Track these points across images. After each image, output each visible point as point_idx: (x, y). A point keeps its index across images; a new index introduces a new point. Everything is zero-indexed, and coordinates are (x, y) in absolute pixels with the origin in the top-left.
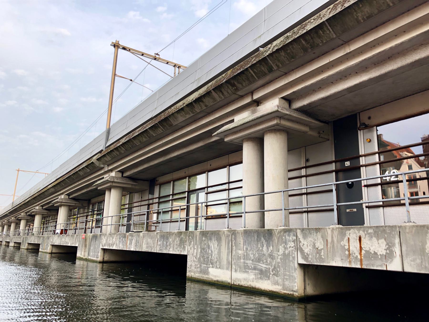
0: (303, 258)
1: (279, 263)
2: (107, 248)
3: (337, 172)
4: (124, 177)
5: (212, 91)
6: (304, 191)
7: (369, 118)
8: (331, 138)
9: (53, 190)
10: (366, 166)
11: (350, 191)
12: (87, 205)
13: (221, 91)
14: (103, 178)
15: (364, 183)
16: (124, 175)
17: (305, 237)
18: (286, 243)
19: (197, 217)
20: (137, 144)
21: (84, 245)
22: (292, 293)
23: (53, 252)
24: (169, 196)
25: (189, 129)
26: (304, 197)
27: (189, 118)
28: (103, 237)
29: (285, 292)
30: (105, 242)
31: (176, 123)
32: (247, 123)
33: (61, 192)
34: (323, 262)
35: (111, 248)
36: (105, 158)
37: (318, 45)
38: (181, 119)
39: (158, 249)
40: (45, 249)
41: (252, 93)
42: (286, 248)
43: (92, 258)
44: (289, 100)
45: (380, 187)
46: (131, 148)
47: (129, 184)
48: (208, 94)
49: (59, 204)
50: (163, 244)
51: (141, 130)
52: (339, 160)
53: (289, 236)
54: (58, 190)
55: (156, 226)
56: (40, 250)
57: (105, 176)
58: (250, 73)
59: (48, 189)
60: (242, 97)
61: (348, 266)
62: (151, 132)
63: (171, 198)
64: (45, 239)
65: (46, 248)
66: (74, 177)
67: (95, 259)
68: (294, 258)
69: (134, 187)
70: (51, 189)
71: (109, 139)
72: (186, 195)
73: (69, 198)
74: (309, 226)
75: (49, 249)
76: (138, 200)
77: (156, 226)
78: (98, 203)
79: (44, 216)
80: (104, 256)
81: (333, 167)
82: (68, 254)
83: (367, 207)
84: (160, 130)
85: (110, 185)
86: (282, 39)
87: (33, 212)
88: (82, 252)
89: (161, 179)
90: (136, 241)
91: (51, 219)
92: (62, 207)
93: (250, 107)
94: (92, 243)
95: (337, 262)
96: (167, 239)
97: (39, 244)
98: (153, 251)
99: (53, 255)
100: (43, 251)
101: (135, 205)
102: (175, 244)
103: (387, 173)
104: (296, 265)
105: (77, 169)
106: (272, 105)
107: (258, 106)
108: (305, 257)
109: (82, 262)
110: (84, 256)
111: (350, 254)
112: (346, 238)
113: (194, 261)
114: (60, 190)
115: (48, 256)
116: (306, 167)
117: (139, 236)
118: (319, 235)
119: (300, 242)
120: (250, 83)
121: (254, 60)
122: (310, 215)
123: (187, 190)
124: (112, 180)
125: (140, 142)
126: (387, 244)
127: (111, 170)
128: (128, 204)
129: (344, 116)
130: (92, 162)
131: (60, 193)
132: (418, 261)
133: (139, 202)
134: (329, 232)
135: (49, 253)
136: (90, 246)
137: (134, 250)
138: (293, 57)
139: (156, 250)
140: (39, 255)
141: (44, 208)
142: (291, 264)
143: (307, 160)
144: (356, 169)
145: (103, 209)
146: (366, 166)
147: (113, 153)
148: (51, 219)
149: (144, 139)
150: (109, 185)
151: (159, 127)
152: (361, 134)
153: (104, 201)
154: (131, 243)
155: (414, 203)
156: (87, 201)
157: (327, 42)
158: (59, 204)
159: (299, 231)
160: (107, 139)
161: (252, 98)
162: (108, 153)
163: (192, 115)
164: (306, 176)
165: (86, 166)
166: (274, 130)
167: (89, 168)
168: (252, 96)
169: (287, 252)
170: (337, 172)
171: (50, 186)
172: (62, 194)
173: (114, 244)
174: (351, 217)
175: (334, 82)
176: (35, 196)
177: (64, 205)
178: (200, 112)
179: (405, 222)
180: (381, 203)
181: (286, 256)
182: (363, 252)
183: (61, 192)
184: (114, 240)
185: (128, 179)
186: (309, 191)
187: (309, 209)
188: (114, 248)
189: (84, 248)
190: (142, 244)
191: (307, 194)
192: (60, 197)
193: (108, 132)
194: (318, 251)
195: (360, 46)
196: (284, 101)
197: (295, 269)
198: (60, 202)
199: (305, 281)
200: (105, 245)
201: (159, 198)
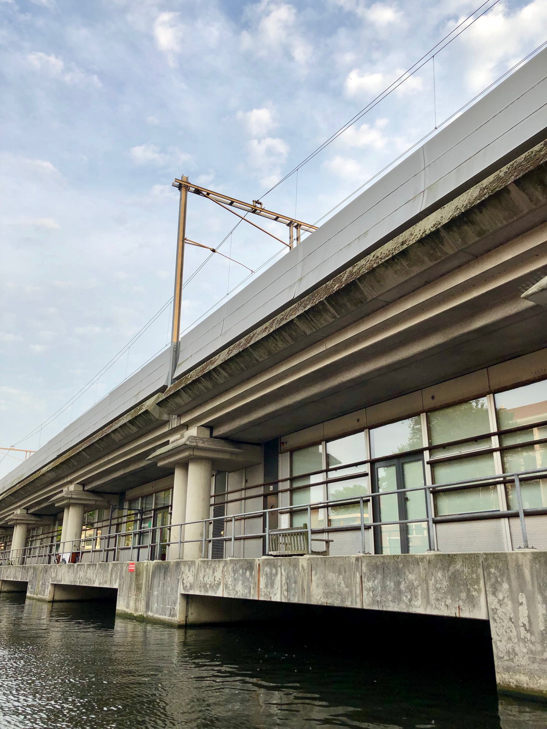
2: (197, 592)
3: (265, 496)
4: (215, 437)
5: (514, 189)
8: (263, 463)
9: (52, 475)
12: (52, 523)
13: (236, 362)
14: (167, 443)
16: (29, 512)
19: (165, 545)
20: (260, 360)
21: (133, 586)
23: (56, 598)
24: (488, 436)
25: (409, 305)
27: (418, 275)
28: (184, 569)
30: (191, 579)
31: (375, 295)
33: (69, 479)
35: (210, 594)
36: (178, 400)
38: (393, 279)
40: (40, 594)
43: (157, 616)
46: (242, 370)
48: (497, 197)
49: (65, 502)
50: (384, 587)
54: (62, 476)
55: (327, 542)
56: (28, 594)
57: (171, 439)
59: (43, 475)
62: (303, 327)
63: (495, 442)
64: (38, 573)
65: (41, 591)
67: (165, 617)
69: (234, 457)
70: (49, 475)
71: (178, 363)
72: (366, 468)
73: (27, 513)
75: (48, 594)
76: (239, 487)
77: (327, 542)
78: (142, 498)
79: (30, 526)
80: (187, 610)
81: (261, 491)
82: (94, 606)
84: (327, 319)
85: (190, 455)
87: (12, 520)
88: (128, 600)
89: (293, 440)
90: (288, 578)
91: (40, 532)
92: (18, 526)
94: (156, 581)
96: (398, 572)
97: (26, 584)
98: (348, 604)
99: (56, 605)
100: (35, 596)
101: (231, 497)
102: (431, 587)
105: (109, 430)
109: (130, 626)
110: (136, 610)
113: (524, 640)
114: (67, 476)
115: (46, 607)
117: (296, 566)
123: (493, 429)
124: (194, 444)
125: (270, 353)
127: (186, 426)
130: (147, 412)
131: (65, 481)
133: (242, 490)
135: (49, 602)
136: (150, 587)
137: (284, 600)
139: (366, 602)
140: (26, 607)
141: (216, 433)
145: (171, 506)
147: (190, 390)
148: (40, 532)
149: (281, 345)
150: (186, 454)
151: (327, 311)
153: (173, 488)
154: (271, 583)
156: (118, 496)
158: (65, 502)
160: (175, 366)
162: (187, 386)
163: (431, 264)
165: (130, 422)
167: (140, 422)
170: (265, 496)
171: (45, 469)
172: (71, 482)
173: (219, 584)
176: (15, 489)
177: (74, 505)
178: (455, 254)
179: (520, 547)
183: (69, 479)
184: (218, 574)
185: (223, 441)
188: (220, 593)
189: (133, 592)
190: (309, 587)
192: (65, 489)
193: (176, 350)
195: (539, 244)
198: (68, 498)
200: (191, 587)
201: (292, 479)
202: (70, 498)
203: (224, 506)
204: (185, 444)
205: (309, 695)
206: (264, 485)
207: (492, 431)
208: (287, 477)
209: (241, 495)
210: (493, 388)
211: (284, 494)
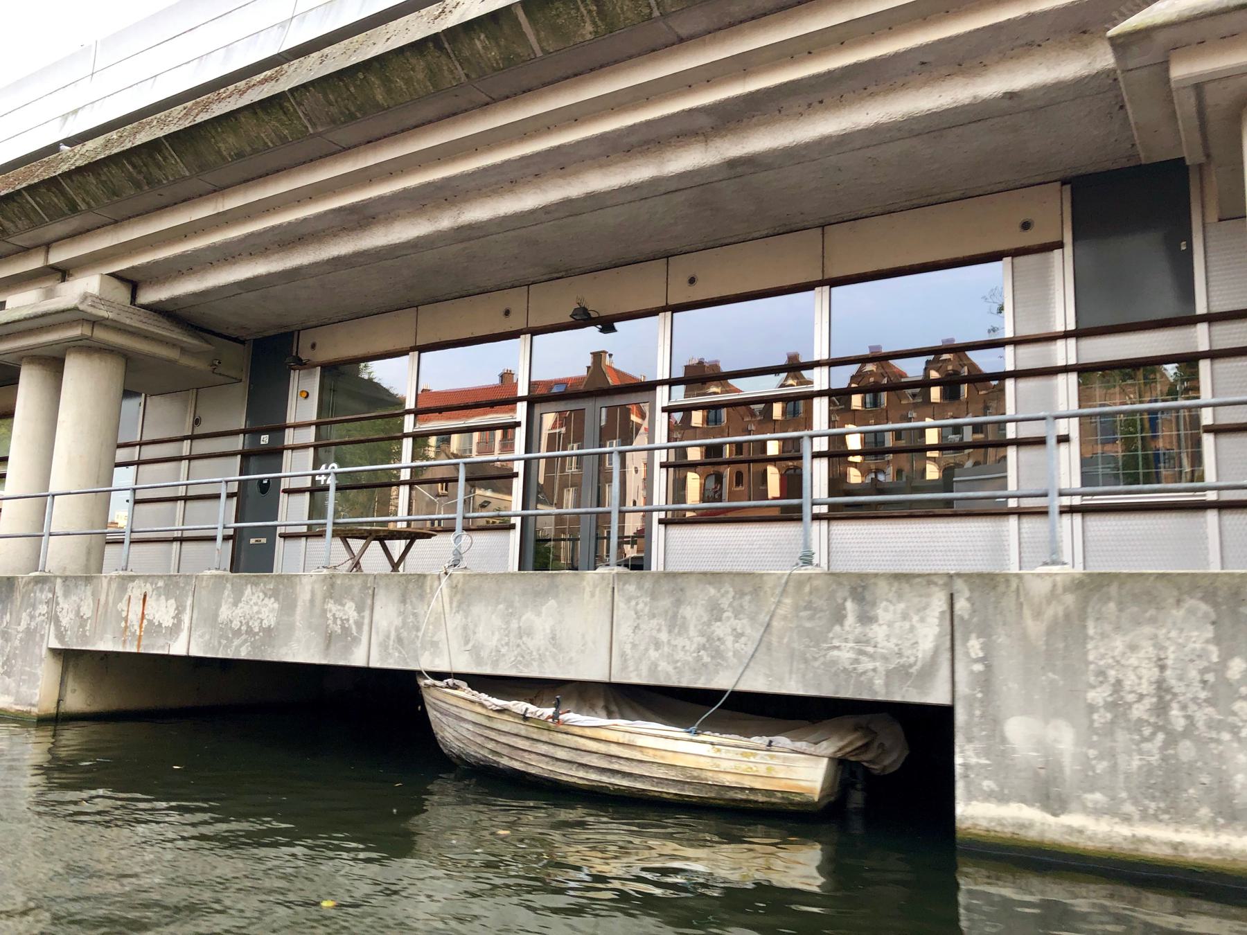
0: (57, 637)
1: (16, 648)
3: (245, 455)
4: (143, 306)
6: (181, 492)
7: (313, 346)
10: (293, 448)
11: (257, 499)
15: (285, 484)
17: (67, 594)
18: (34, 607)
22: (28, 708)
26: (180, 504)
29: (18, 708)
32: (14, 322)
34: (87, 644)
35: (914, 697)
37: (160, 182)
39: (645, 672)
41: (47, 246)
42: (32, 617)
44: (132, 282)
45: (307, 495)
47: (167, 347)
51: (177, 121)
52: (252, 432)
53: (42, 591)
58: (28, 202)
60: (24, 251)
61: (121, 649)
66: (266, 130)
68: (42, 636)
74: (1090, 563)
81: (238, 443)
83: (661, 522)
86: (100, 140)
93: (43, 281)
95: (106, 644)
103: (323, 469)
104: (44, 651)
106: (83, 288)
107: (63, 280)
108: (60, 636)
111: (126, 627)
112: (126, 597)
116: (192, 438)
118: (89, 589)
119: (58, 604)
120: (34, 226)
121: (41, 173)
122: (187, 546)
126: (177, 608)
128: (318, 425)
129: (272, 333)
132: (207, 637)
134: (105, 582)
138: (115, 194)
141: (149, 296)
142: (37, 651)
143: (197, 422)
144: (274, 454)
146: (293, 448)
152: (294, 376)
155: (837, 514)
157: (174, 182)
159: (59, 581)
161: (47, 259)
164: (190, 458)
166: (87, 348)
168: (47, 252)
169: (33, 625)
170: (245, 455)
174: (251, 555)
175: (195, 268)
180: (304, 529)
181: (30, 633)
182: (145, 622)
186: (193, 492)
187: (186, 534)
191: (186, 499)
194: (82, 621)
196: (116, 283)
197: (42, 660)
199: (62, 683)
202: (95, 322)
203: (1002, 390)
204: (75, 309)
205: (129, 795)
206: (244, 432)
207: (659, 378)
208: (236, 428)
209: (181, 449)
210: (673, 301)
211: (297, 453)
